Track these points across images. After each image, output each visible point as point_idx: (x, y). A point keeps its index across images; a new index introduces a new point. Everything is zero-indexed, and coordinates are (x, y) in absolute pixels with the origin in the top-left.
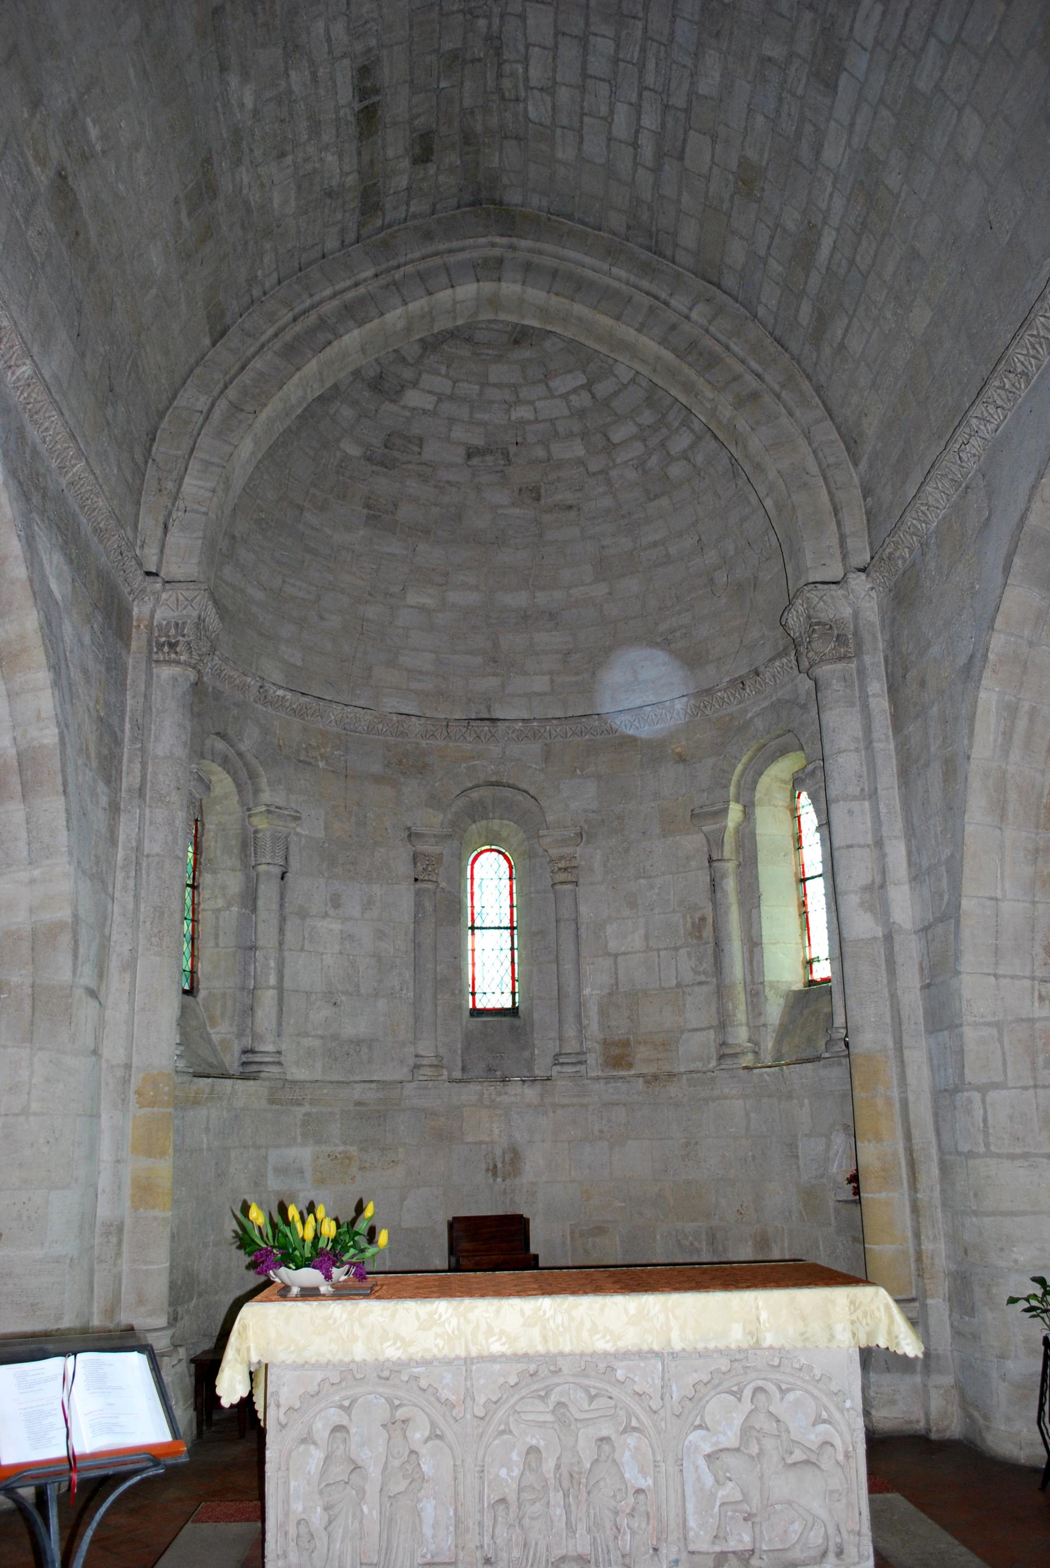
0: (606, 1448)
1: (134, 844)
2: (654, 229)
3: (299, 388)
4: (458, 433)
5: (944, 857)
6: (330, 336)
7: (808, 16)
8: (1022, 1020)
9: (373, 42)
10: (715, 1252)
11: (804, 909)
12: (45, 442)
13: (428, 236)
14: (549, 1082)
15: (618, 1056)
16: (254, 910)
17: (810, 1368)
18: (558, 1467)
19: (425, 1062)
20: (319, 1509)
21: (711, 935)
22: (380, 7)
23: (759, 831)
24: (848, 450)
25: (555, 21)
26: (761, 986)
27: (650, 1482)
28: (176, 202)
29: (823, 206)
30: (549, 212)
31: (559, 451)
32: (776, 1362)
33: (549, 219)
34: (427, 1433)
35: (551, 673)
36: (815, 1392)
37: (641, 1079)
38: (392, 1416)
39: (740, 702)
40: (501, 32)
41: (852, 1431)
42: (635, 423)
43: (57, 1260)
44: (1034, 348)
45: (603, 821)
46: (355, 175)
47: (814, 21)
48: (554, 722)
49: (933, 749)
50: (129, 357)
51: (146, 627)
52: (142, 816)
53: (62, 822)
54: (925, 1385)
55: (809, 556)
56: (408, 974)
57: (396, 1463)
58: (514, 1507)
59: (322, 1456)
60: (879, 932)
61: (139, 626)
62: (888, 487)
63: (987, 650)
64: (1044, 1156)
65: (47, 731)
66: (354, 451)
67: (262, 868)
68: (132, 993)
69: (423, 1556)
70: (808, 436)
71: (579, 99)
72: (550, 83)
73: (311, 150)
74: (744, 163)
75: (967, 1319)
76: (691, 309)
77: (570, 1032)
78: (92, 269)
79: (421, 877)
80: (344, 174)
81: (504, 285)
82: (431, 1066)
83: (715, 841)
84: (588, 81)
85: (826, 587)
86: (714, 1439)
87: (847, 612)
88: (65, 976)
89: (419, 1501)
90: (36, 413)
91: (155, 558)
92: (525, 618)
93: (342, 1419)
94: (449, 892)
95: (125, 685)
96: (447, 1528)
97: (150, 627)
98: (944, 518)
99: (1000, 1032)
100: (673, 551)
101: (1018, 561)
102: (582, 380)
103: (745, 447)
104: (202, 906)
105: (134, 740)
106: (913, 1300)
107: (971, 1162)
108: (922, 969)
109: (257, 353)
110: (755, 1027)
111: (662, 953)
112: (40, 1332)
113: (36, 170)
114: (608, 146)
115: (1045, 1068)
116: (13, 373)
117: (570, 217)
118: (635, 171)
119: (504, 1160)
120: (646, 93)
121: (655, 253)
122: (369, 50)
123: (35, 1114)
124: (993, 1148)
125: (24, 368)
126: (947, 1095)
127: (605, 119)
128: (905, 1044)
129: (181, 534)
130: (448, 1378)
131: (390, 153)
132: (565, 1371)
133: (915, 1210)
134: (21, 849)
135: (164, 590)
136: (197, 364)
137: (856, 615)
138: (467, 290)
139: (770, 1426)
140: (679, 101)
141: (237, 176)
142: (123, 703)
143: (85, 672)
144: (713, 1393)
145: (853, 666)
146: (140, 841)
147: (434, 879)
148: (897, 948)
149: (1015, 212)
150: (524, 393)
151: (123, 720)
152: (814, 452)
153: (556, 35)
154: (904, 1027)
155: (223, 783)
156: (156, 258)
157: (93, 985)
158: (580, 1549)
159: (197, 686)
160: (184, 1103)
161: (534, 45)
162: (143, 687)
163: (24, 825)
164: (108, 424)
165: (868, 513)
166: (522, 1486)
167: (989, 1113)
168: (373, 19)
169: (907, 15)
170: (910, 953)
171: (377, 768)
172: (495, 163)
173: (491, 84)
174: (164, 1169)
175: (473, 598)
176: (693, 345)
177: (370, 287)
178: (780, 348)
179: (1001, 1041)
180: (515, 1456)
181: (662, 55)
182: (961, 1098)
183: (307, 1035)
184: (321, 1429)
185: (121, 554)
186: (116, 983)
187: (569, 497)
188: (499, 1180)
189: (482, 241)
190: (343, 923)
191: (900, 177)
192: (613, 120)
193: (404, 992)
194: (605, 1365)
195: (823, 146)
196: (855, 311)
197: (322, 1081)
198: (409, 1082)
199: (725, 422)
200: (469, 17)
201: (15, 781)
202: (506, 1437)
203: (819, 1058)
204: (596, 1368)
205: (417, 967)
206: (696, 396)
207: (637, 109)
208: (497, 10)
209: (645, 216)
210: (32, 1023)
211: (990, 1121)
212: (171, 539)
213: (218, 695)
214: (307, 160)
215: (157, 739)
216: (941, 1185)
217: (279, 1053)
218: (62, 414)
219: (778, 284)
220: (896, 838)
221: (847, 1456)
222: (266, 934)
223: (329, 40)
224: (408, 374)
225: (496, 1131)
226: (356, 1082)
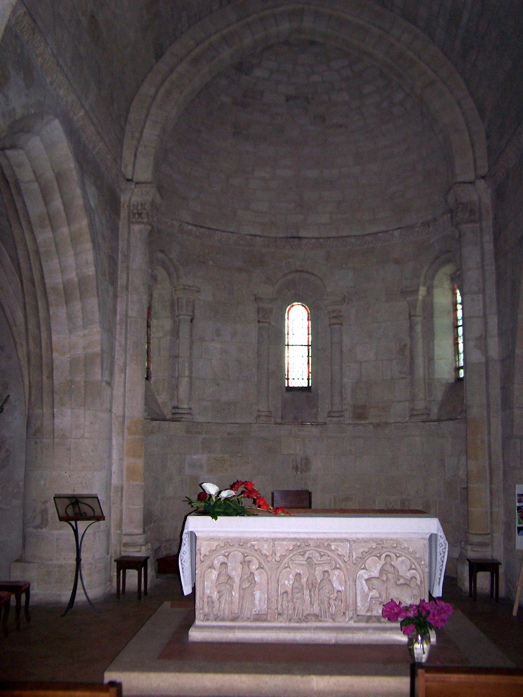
0: (326, 574)
11: (456, 342)
14: (324, 426)
15: (360, 413)
16: (178, 337)
18: (307, 581)
20: (216, 593)
23: (434, 301)
27: (343, 588)
32: (395, 545)
34: (257, 567)
36: (410, 557)
38: (244, 560)
41: (423, 573)
53: (96, 308)
57: (245, 577)
58: (290, 595)
59: (217, 573)
60: (483, 360)
67: (182, 317)
69: (255, 611)
77: (337, 400)
79: (261, 320)
83: (413, 305)
86: (369, 574)
87: (475, 198)
88: (98, 377)
89: (254, 591)
91: (131, 173)
93: (225, 560)
96: (264, 602)
97: (129, 206)
104: (152, 336)
111: (384, 362)
119: (301, 464)
130: (266, 546)
132: (311, 545)
134: (80, 322)
139: (391, 570)
142: (118, 245)
146: (127, 311)
155: (161, 274)
158: (315, 612)
166: (294, 586)
170: (496, 370)
174: (140, 463)
180: (291, 576)
184: (216, 563)
186: (118, 378)
188: (299, 473)
202: (288, 569)
203: (456, 419)
204: (324, 545)
210: (85, 398)
217: (190, 409)
221: (421, 583)
222: (184, 351)
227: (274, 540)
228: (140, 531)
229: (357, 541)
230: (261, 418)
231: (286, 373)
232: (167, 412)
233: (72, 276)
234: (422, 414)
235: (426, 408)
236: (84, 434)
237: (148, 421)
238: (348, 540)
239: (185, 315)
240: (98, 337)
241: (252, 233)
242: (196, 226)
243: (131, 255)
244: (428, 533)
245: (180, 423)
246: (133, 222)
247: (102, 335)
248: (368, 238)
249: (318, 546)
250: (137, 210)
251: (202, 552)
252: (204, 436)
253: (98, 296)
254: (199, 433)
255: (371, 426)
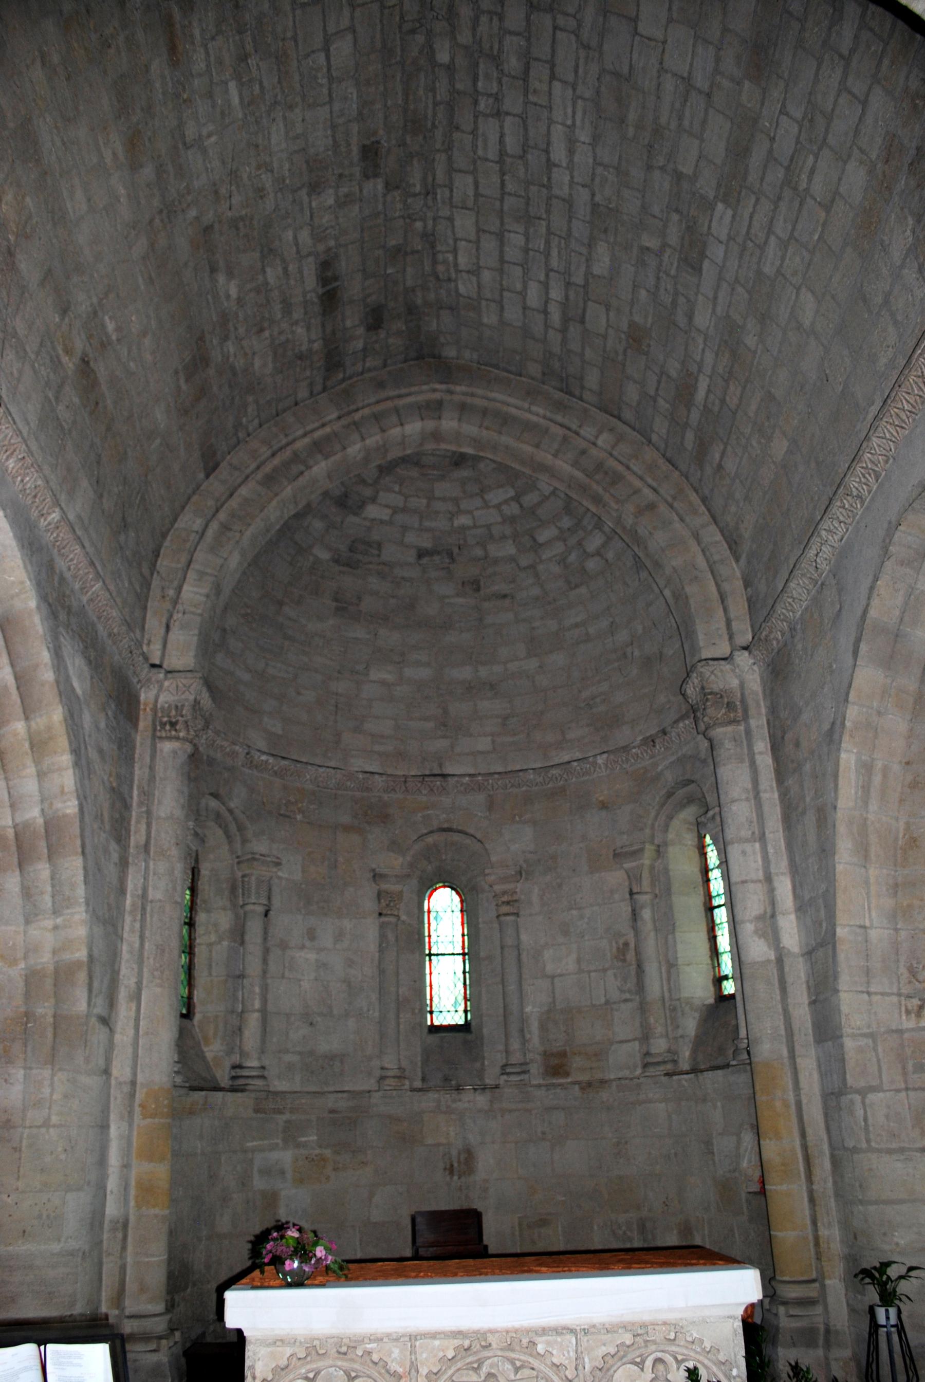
1: (140, 892)
2: (564, 375)
3: (275, 513)
4: (411, 538)
5: (821, 892)
6: (302, 468)
7: (675, 217)
8: (893, 1031)
9: (332, 243)
10: (645, 1240)
12: (69, 569)
13: (381, 385)
14: (497, 1090)
15: (556, 1066)
16: (242, 943)
17: (701, 1341)
19: (390, 1073)
21: (634, 959)
22: (337, 218)
23: (671, 867)
24: (730, 548)
25: (477, 222)
26: (678, 1002)
27: (203, 801)
28: (176, 372)
29: (698, 358)
30: (478, 363)
31: (494, 550)
32: (672, 1336)
33: (479, 369)
35: (492, 735)
37: (577, 1087)
39: (651, 757)
40: (434, 230)
42: (557, 527)
43: (72, 1254)
44: (864, 477)
45: (539, 861)
46: (321, 342)
47: (681, 221)
48: (496, 776)
49: (808, 799)
50: (138, 493)
51: (151, 710)
52: (147, 868)
53: (80, 878)
54: (827, 1358)
55: (701, 637)
56: (374, 997)
60: (772, 956)
61: (145, 709)
62: (763, 581)
63: (845, 719)
64: (917, 1150)
65: (69, 803)
66: (324, 555)
67: (249, 907)
68: (137, 1019)
70: (697, 537)
71: (499, 279)
72: (475, 268)
73: (284, 325)
74: (632, 324)
75: (859, 1297)
76: (597, 437)
77: (515, 1045)
78: (109, 429)
79: (384, 912)
80: (311, 341)
81: (444, 422)
82: (394, 1077)
84: (506, 265)
85: (716, 662)
87: (735, 683)
88: (82, 1006)
90: (64, 548)
91: (159, 653)
92: (471, 689)
94: (409, 924)
95: (134, 759)
97: (155, 710)
98: (806, 609)
99: (874, 1042)
100: (591, 630)
101: (863, 647)
102: (511, 493)
103: (646, 548)
104: (198, 941)
105: (141, 803)
106: (814, 1281)
107: (856, 1156)
108: (809, 988)
109: (243, 482)
110: (676, 1038)
111: (593, 974)
112: (55, 1318)
113: (65, 359)
114: (524, 313)
115: (913, 1073)
116: (45, 520)
117: (496, 366)
118: (546, 333)
120: (552, 274)
121: (566, 393)
122: (330, 249)
123: (54, 1126)
124: (873, 1144)
125: (54, 515)
126: (834, 1096)
127: (520, 293)
128: (797, 1053)
129: (181, 632)
130: (396, 1353)
131: (349, 323)
132: (494, 1346)
133: (812, 1200)
135: (166, 678)
136: (194, 493)
137: (742, 685)
138: (414, 427)
140: (578, 279)
141: (225, 350)
142: (132, 774)
143: (101, 752)
144: (619, 1364)
145: (742, 728)
146: (145, 889)
147: (396, 913)
148: (787, 969)
149: (845, 368)
150: (464, 505)
151: (131, 788)
152: (703, 551)
153: (478, 232)
154: (795, 1038)
155: (215, 835)
156: (159, 415)
157: (104, 1013)
159: (194, 757)
160: (178, 1114)
161: (461, 240)
162: (148, 759)
163: (50, 882)
164: (121, 548)
165: (749, 600)
167: (869, 1114)
168: (332, 227)
169: (751, 218)
170: (798, 972)
171: (346, 819)
172: (434, 326)
173: (428, 268)
174: (161, 1171)
175: (424, 673)
176: (600, 466)
177: (334, 427)
178: (671, 467)
179: (875, 1050)
181: (563, 245)
182: (844, 1100)
183: (287, 1051)
185: (131, 652)
186: (124, 1012)
187: (503, 588)
188: (456, 1178)
189: (425, 387)
190: (318, 953)
191: (756, 338)
192: (526, 294)
193: (371, 1012)
194: (528, 1340)
195: (694, 313)
196: (728, 439)
197: (300, 1092)
198: (376, 1091)
199: (628, 527)
200: (408, 220)
201: (42, 845)
203: (728, 1066)
204: (520, 1343)
205: (382, 991)
206: (604, 507)
207: (546, 286)
208: (430, 214)
209: (557, 365)
210: (53, 1048)
211: (870, 1121)
212: (172, 636)
213: (211, 762)
214: (280, 333)
215: (160, 803)
216: (833, 1177)
218: (84, 547)
219: (666, 417)
220: (782, 874)
222: (253, 966)
223: (297, 245)
224: (368, 492)
225: (452, 1134)
226: (330, 1092)
227: (413, 1337)
228: (160, 1307)
229: (592, 1330)
230: (387, 1082)
231: (428, 1002)
232: (223, 1076)
233: (33, 813)
234: (665, 1062)
235: (669, 1051)
236: (49, 1118)
237: (183, 1091)
238: (572, 1331)
239: (254, 904)
240: (82, 932)
241: (367, 769)
242: (273, 755)
243: (157, 793)
244: (741, 1304)
245: (245, 1094)
246: (161, 738)
247: (91, 928)
248: (554, 772)
249: (510, 1347)
250: (169, 717)
251: (258, 1374)
252: (287, 1116)
253: (83, 853)
254: (280, 1112)
255: (577, 1087)
